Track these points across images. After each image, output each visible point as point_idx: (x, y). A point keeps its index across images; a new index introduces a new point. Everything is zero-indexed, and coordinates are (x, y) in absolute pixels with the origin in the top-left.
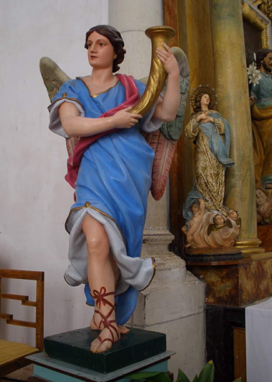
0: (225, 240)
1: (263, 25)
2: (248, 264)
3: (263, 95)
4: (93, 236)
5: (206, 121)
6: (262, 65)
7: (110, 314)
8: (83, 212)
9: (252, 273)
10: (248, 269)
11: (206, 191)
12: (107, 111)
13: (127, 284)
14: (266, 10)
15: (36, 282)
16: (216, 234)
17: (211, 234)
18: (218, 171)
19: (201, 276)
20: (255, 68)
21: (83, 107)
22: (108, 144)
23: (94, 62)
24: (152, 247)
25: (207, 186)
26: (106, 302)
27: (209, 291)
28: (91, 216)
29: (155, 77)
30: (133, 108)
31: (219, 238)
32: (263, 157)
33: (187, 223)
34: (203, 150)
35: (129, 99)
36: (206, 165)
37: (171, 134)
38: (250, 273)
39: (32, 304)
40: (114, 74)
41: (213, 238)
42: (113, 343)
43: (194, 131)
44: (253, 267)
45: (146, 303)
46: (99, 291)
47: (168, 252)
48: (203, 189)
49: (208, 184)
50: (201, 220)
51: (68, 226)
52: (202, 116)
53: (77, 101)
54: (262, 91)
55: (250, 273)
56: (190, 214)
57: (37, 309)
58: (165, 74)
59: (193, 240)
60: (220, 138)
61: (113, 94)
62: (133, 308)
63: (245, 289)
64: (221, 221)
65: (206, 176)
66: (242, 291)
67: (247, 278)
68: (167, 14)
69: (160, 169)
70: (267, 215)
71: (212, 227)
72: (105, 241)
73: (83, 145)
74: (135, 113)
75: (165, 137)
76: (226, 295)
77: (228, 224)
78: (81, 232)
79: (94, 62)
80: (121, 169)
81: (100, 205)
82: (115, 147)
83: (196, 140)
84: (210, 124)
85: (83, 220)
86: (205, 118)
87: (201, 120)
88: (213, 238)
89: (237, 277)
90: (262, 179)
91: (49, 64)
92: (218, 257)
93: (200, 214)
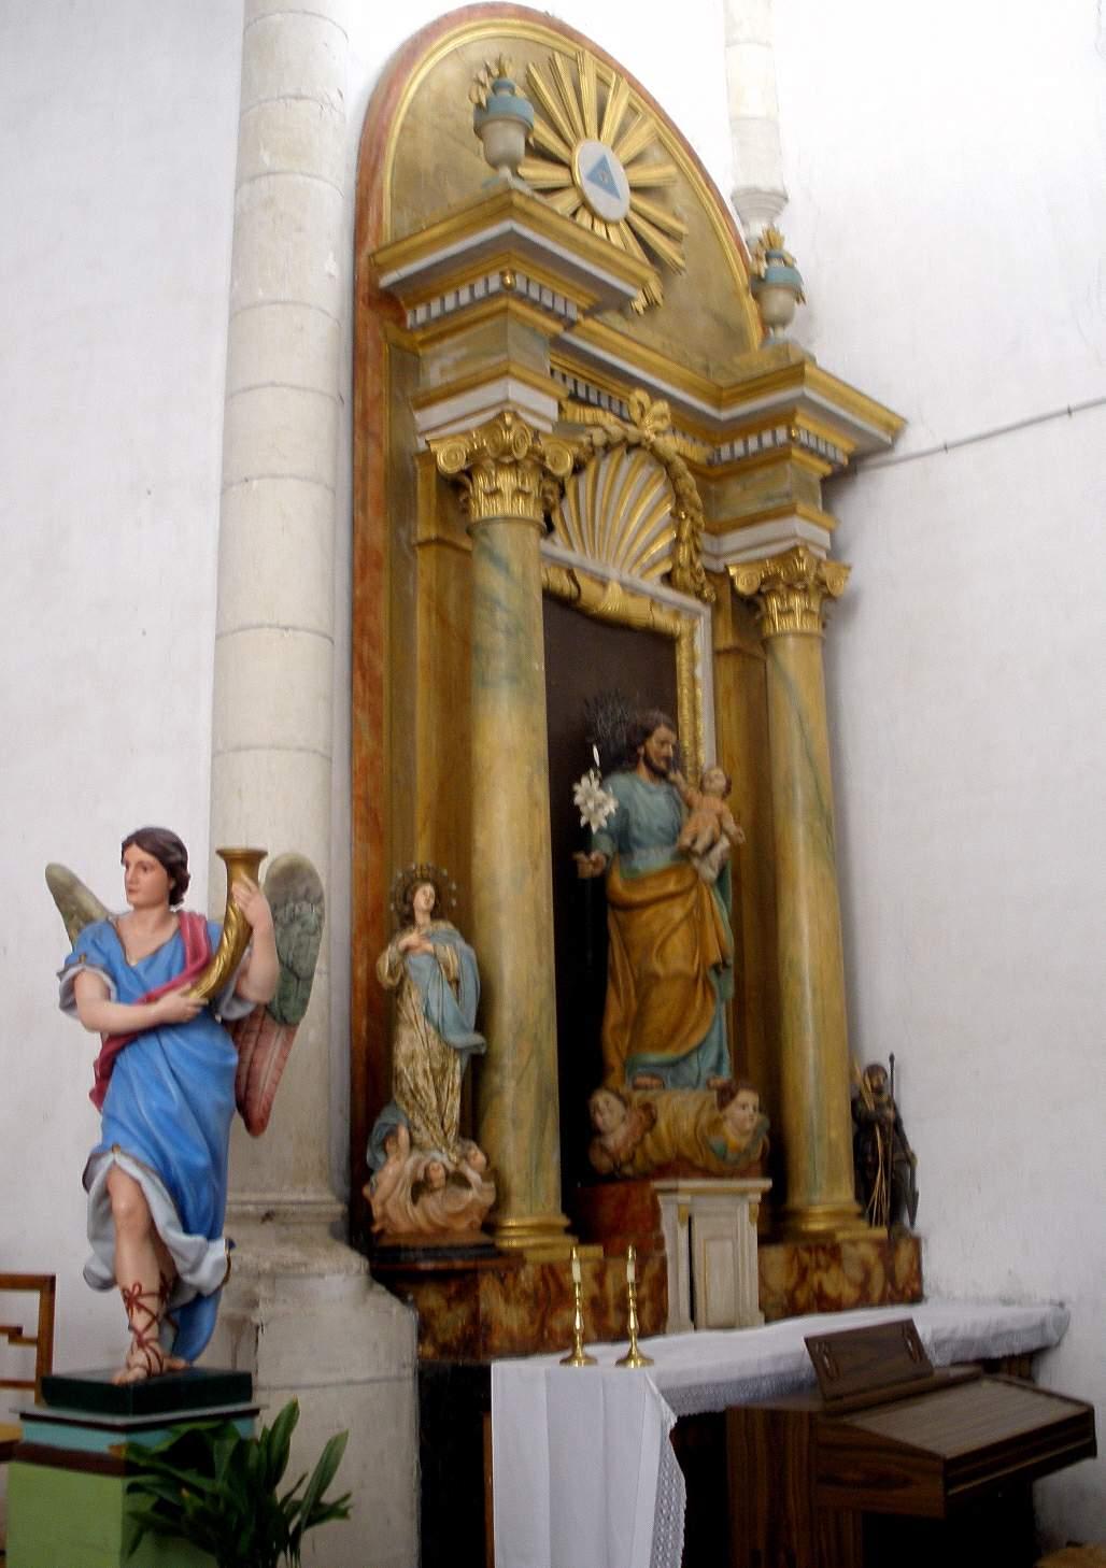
0: (457, 1215)
1: (679, 627)
2: (510, 1268)
3: (639, 844)
4: (122, 1201)
5: (418, 951)
6: (641, 758)
7: (148, 1326)
8: (107, 1161)
9: (524, 1292)
10: (510, 1281)
11: (413, 1108)
12: (153, 990)
13: (191, 1286)
14: (691, 583)
15: (39, 1298)
16: (430, 1203)
17: (419, 1203)
18: (443, 1065)
19: (410, 1297)
20: (596, 784)
21: (114, 979)
22: (150, 1046)
23: (134, 898)
24: (287, 1229)
25: (414, 1097)
26: (141, 1307)
27: (424, 1330)
28: (120, 1169)
29: (229, 933)
30: (195, 986)
31: (438, 1212)
32: (634, 1005)
33: (373, 1179)
34: (410, 1019)
35: (191, 968)
36: (414, 1051)
37: (285, 1012)
38: (518, 1290)
39: (30, 1341)
40: (174, 909)
41: (425, 1213)
42: (149, 1373)
43: (392, 973)
44: (527, 1279)
45: (260, 1341)
46: (131, 1289)
47: (329, 1240)
48: (407, 1104)
49: (419, 1092)
50: (402, 1169)
51: (87, 1181)
52: (411, 938)
53: (105, 970)
54: (635, 832)
55: (518, 1290)
56: (381, 1157)
57: (38, 1351)
58: (247, 931)
59: (385, 1216)
60: (449, 992)
61: (165, 956)
62: (206, 1333)
63: (501, 1324)
64: (438, 1175)
65: (414, 1075)
66: (489, 1328)
67: (507, 1300)
68: (358, 675)
69: (262, 1083)
70: (623, 1156)
71: (420, 1188)
72: (140, 1211)
73: (113, 1046)
74: (196, 997)
75: (275, 1018)
76: (456, 1338)
77: (458, 1179)
78: (105, 1194)
79: (134, 898)
80: (169, 1091)
81: (135, 1150)
82: (164, 1053)
83: (397, 991)
84: (426, 957)
85: (110, 1171)
86: (416, 944)
87: (407, 950)
88: (425, 1213)
89: (477, 1299)
90: (625, 1065)
91: (62, 879)
92: (432, 1252)
93: (398, 1158)
